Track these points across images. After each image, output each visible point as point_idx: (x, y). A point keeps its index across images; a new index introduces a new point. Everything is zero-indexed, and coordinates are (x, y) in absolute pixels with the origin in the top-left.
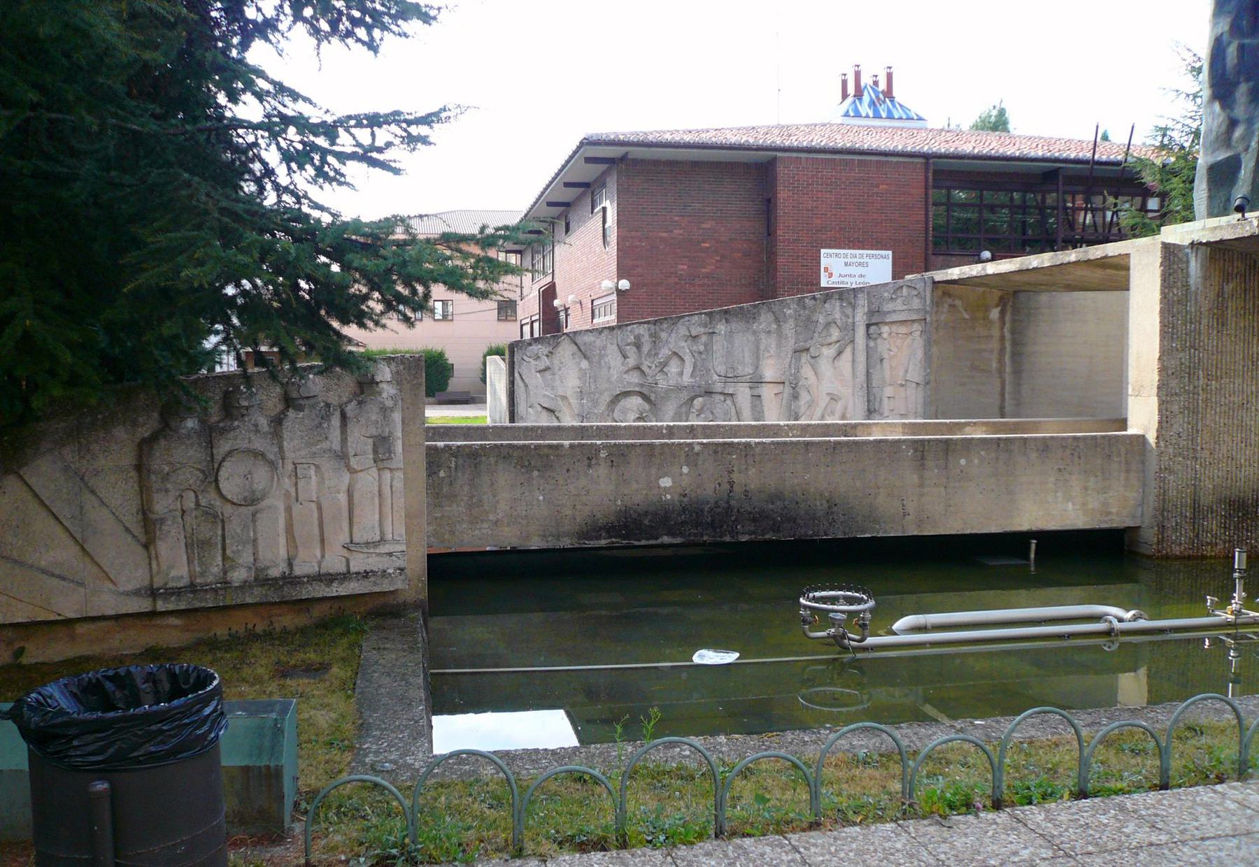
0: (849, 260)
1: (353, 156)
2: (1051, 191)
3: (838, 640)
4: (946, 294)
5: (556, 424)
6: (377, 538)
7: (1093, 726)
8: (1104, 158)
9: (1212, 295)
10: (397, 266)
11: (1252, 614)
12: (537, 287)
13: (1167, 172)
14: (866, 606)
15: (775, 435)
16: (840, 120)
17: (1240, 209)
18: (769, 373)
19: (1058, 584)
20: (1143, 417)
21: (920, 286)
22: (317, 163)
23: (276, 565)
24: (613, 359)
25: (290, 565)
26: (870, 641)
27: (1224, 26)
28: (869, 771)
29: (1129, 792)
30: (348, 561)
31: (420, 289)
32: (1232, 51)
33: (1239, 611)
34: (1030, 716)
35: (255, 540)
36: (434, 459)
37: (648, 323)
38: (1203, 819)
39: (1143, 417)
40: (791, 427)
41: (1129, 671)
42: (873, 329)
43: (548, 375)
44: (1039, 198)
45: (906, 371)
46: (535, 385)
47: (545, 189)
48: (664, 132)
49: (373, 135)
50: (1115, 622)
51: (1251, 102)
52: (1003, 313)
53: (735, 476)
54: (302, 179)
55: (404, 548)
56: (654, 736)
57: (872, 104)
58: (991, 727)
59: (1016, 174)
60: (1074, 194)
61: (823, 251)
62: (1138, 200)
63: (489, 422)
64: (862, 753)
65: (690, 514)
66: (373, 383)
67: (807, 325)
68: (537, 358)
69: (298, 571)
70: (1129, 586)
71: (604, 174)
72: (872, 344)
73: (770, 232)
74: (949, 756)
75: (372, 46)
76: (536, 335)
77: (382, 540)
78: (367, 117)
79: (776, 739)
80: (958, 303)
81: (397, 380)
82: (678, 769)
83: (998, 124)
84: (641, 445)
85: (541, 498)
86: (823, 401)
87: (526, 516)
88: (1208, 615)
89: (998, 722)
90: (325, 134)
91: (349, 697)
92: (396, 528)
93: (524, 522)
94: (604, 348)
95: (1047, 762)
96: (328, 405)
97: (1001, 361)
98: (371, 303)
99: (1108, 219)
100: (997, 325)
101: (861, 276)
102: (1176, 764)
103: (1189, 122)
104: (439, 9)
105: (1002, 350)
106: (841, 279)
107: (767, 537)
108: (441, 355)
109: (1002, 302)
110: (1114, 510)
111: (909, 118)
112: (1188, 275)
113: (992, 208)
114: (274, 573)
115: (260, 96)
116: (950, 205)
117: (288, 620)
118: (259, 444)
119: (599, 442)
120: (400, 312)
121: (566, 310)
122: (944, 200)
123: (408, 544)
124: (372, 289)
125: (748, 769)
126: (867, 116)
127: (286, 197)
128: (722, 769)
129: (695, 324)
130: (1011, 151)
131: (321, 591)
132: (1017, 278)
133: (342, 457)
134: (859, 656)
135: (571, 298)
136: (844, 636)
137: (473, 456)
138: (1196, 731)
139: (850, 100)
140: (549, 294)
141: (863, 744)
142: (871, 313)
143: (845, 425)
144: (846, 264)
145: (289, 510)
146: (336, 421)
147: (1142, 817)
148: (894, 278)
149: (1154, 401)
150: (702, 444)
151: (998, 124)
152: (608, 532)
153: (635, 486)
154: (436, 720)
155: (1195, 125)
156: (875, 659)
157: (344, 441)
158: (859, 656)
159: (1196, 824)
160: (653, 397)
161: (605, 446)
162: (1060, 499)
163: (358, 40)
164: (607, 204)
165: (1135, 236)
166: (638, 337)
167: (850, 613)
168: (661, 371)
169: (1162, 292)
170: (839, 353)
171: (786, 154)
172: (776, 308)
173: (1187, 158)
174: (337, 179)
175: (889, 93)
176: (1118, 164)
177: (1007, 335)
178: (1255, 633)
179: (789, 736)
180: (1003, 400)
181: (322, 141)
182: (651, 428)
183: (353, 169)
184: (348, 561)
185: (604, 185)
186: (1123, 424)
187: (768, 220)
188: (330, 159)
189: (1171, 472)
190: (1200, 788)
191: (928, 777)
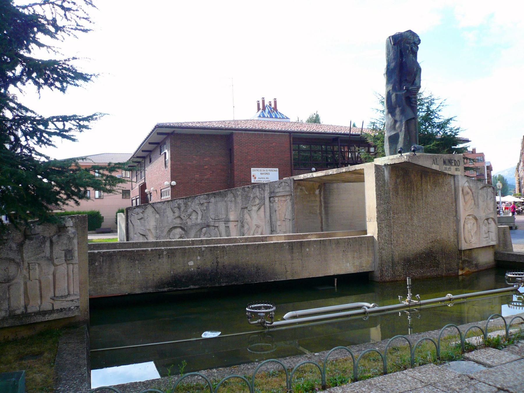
0: (262, 172)
1: (55, 134)
2: (335, 145)
3: (262, 324)
4: (299, 185)
5: (146, 241)
6: (67, 294)
7: (357, 352)
8: (354, 133)
9: (393, 184)
10: (74, 178)
11: (415, 301)
12: (138, 184)
13: (376, 138)
14: (272, 309)
15: (235, 242)
16: (257, 119)
17: (400, 152)
18: (232, 217)
19: (346, 295)
20: (372, 229)
21: (289, 182)
22: (39, 135)
23: (19, 309)
24: (169, 213)
25: (26, 307)
26: (275, 323)
27: (390, 88)
28: (274, 379)
29: (373, 377)
30: (53, 304)
31: (82, 189)
32: (393, 96)
33: (410, 301)
34: (336, 350)
35: (9, 298)
36: (92, 258)
37: (183, 199)
38: (400, 385)
39: (372, 229)
40: (241, 239)
41: (374, 327)
42: (272, 199)
43: (142, 221)
44: (332, 148)
45: (285, 215)
46: (137, 225)
47: (141, 145)
48: (189, 123)
49: (64, 125)
50: (367, 309)
51: (401, 114)
52: (320, 191)
53: (219, 260)
54: (32, 143)
55: (78, 297)
56: (184, 373)
57: (269, 112)
58: (321, 355)
59: (323, 139)
60: (344, 146)
62: (367, 148)
63: (118, 241)
64: (271, 371)
65: (201, 276)
66: (65, 227)
67: (246, 198)
68: (138, 214)
69: (29, 311)
70: (371, 294)
71: (165, 139)
72: (271, 205)
73: (231, 161)
74: (306, 369)
75: (63, 90)
76: (138, 204)
77: (69, 294)
78: (61, 117)
79: (237, 369)
80: (304, 188)
81: (75, 226)
82: (196, 385)
83: (316, 120)
84: (180, 248)
85: (139, 272)
86: (254, 228)
87: (133, 280)
88: (400, 303)
89: (324, 353)
90: (43, 125)
91: (52, 366)
92: (75, 289)
93: (132, 283)
94: (165, 209)
95: (343, 368)
96: (44, 237)
97: (320, 209)
98: (61, 195)
99: (357, 155)
100: (318, 196)
101: (267, 178)
102: (389, 363)
103: (382, 120)
104: (91, 75)
105: (321, 205)
107: (233, 283)
108: (98, 213)
109: (320, 187)
110: (364, 265)
111: (283, 118)
112: (384, 176)
113: (315, 152)
114: (18, 312)
115: (11, 109)
116: (300, 150)
117: (25, 333)
118: (12, 255)
119: (163, 248)
120: (73, 199)
121: (150, 194)
122: (297, 148)
123: (80, 295)
124: (61, 190)
125: (226, 382)
126: (268, 117)
127: (24, 150)
128: (214, 384)
129: (202, 198)
130: (321, 130)
131: (40, 319)
132: (325, 178)
133: (51, 259)
134: (270, 330)
135: (152, 189)
136: (264, 322)
137: (110, 256)
138: (396, 349)
139: (261, 111)
140: (143, 187)
141: (271, 366)
142: (271, 193)
143: (262, 237)
144: (261, 174)
145: (25, 284)
146: (48, 244)
147: (377, 387)
148: (279, 179)
149: (376, 223)
150: (205, 247)
151: (316, 120)
152: (168, 285)
153: (178, 266)
154: (93, 372)
155: (384, 122)
156: (277, 331)
157: (51, 252)
158: (270, 330)
159: (397, 387)
160: (186, 228)
161: (166, 250)
163: (56, 87)
164: (166, 151)
165: (366, 162)
166: (179, 205)
167: (266, 313)
168: (189, 218)
169: (376, 183)
170: (259, 209)
171: (237, 132)
172: (234, 192)
173: (381, 133)
174: (48, 143)
175: (275, 108)
176: (359, 135)
177: (322, 199)
178: (416, 309)
179: (242, 366)
180: (322, 225)
181: (41, 127)
182: (185, 241)
183: (55, 139)
184: (53, 304)
185: (165, 144)
186: (365, 232)
187: (230, 157)
188: (44, 134)
189: (384, 249)
190: (398, 373)
191: (297, 378)
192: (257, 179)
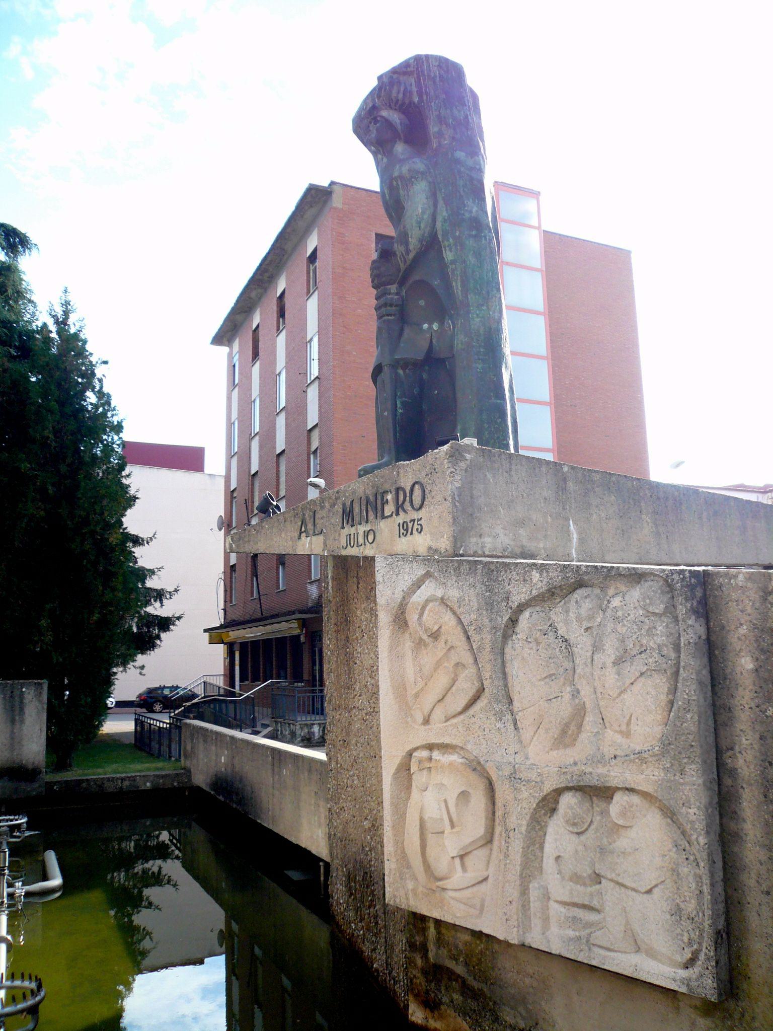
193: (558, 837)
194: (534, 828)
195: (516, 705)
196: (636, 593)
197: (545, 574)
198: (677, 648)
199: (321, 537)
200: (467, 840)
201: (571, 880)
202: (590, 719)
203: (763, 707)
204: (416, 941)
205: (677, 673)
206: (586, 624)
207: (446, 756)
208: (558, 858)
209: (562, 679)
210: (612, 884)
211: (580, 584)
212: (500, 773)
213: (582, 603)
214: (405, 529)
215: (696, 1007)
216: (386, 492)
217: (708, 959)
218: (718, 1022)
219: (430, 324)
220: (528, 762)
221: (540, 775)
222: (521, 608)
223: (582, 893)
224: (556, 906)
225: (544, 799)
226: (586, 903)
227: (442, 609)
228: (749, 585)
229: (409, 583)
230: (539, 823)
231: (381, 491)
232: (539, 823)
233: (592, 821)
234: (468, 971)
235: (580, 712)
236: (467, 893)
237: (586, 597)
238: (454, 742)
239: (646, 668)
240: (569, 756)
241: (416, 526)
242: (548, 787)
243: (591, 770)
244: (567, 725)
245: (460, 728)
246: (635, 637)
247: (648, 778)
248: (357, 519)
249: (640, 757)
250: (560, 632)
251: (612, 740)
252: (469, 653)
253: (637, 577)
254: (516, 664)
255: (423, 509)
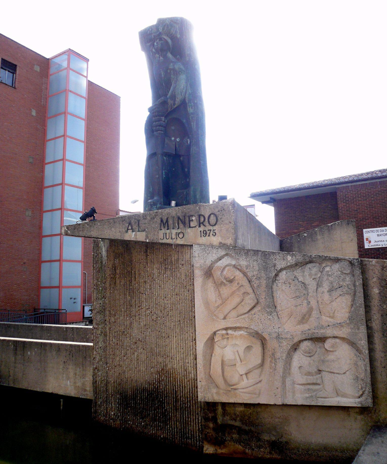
0: (380, 233)
61: (364, 230)
106: (376, 243)
112: (102, 257)
144: (378, 235)
162: (64, 378)
192: (373, 243)
193: (298, 359)
194: (287, 357)
195: (278, 308)
196: (336, 266)
197: (294, 257)
198: (355, 286)
199: (144, 233)
200: (250, 366)
201: (305, 375)
202: (315, 313)
203: (382, 305)
204: (209, 417)
205: (355, 294)
206: (313, 277)
207: (237, 332)
208: (300, 367)
209: (303, 298)
210: (327, 373)
211: (311, 262)
212: (271, 336)
213: (313, 269)
214: (205, 234)
215: (357, 412)
216: (192, 216)
217: (369, 392)
218: (366, 415)
219: (176, 138)
220: (286, 331)
221: (291, 335)
222: (281, 270)
223: (311, 379)
224: (298, 386)
225: (294, 345)
226: (315, 382)
227: (234, 269)
228: (377, 265)
229: (216, 257)
230: (289, 354)
231: (188, 215)
232: (289, 354)
233: (316, 351)
234: (242, 424)
235: (310, 310)
236: (251, 388)
237: (314, 267)
238: (243, 326)
239: (342, 293)
240: (306, 327)
241: (212, 233)
242: (296, 340)
243: (317, 331)
244: (305, 315)
245: (247, 320)
246: (337, 282)
247: (344, 332)
248: (172, 226)
249: (341, 325)
250: (300, 280)
251: (325, 320)
252: (251, 288)
253: (337, 260)
254: (279, 292)
255: (216, 226)
